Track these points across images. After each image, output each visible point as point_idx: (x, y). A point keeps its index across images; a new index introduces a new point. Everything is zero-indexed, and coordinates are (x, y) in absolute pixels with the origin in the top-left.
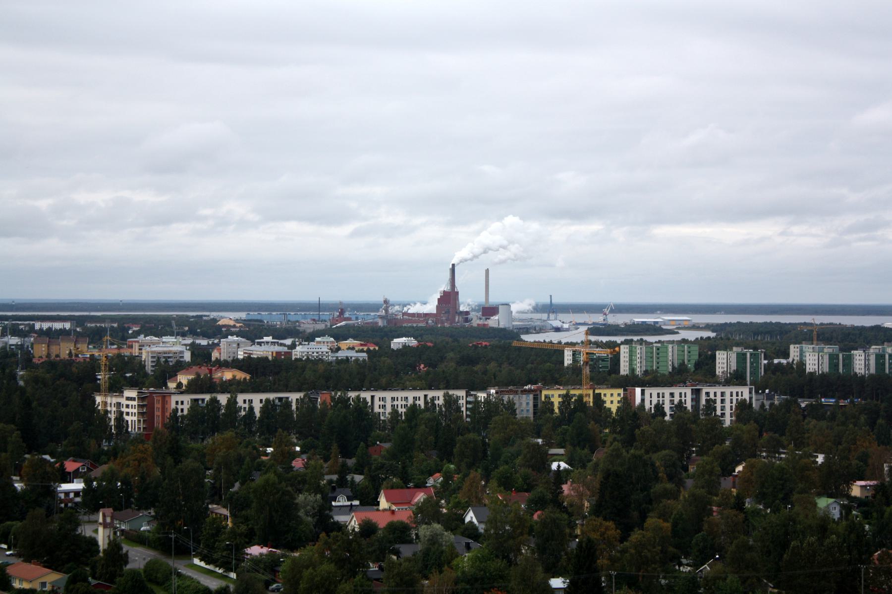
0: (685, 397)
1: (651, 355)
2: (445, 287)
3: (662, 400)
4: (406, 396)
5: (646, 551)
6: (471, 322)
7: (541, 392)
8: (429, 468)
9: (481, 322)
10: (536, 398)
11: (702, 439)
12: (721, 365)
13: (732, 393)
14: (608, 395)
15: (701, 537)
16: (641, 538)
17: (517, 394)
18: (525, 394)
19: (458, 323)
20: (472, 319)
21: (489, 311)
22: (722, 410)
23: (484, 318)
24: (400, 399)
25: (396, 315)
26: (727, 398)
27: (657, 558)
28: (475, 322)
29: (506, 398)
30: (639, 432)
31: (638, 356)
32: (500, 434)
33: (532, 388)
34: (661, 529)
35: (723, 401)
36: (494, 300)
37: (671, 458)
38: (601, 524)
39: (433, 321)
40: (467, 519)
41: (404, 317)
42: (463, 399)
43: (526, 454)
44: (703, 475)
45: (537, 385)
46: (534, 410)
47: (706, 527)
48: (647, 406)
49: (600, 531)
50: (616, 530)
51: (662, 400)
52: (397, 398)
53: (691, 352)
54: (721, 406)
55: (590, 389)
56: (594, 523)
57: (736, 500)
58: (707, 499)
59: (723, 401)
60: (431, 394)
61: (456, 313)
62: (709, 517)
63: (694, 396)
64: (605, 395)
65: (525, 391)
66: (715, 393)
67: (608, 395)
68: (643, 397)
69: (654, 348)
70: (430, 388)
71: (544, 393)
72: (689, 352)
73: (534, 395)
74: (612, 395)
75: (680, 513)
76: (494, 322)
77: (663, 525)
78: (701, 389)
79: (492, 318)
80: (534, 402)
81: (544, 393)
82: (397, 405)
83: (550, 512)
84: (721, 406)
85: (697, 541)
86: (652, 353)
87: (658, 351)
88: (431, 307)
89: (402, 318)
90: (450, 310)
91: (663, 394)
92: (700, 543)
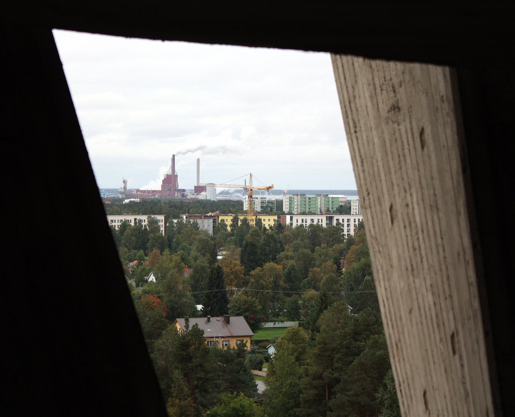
0: (322, 222)
1: (304, 203)
2: (166, 170)
3: (305, 224)
4: (121, 219)
5: (262, 280)
6: (187, 197)
7: (218, 217)
8: (130, 258)
9: (193, 197)
10: (214, 222)
11: (326, 241)
12: (354, 211)
13: (355, 219)
14: (267, 220)
15: (306, 281)
16: (258, 272)
17: (201, 219)
18: (207, 219)
19: (177, 197)
20: (187, 195)
21: (199, 189)
22: (348, 232)
23: (196, 194)
24: (117, 221)
25: (132, 191)
26: (352, 223)
27: (270, 286)
28: (190, 196)
29: (192, 221)
30: (282, 236)
31: (296, 204)
32: (186, 241)
33: (212, 215)
34: (276, 269)
35: (348, 225)
36: (203, 182)
37: (299, 245)
38: (231, 262)
39: (159, 196)
40: (150, 280)
41: (138, 193)
42: (162, 222)
43: (199, 246)
44: (320, 256)
45: (216, 213)
46: (213, 230)
47: (310, 274)
48: (294, 225)
49: (230, 267)
50: (241, 266)
51: (305, 224)
52: (115, 220)
53: (334, 202)
54: (347, 229)
55: (254, 215)
56: (227, 261)
57: (335, 261)
58: (312, 256)
59: (348, 225)
60: (139, 217)
61: (176, 190)
62: (312, 268)
63: (328, 222)
64: (264, 220)
65: (207, 216)
66: (343, 220)
67: (267, 220)
68: (292, 221)
69: (307, 198)
70: (139, 214)
71: (221, 218)
72: (333, 202)
73: (213, 220)
74: (269, 220)
75: (293, 266)
76: (202, 196)
77: (277, 267)
78: (333, 217)
79: (201, 193)
80: (213, 225)
81: (221, 218)
82: (115, 225)
83: (201, 262)
84: (347, 229)
85: (304, 284)
86: (305, 201)
87: (310, 200)
88: (156, 185)
89: (136, 193)
90: (171, 188)
91: (306, 219)
92: (306, 285)
